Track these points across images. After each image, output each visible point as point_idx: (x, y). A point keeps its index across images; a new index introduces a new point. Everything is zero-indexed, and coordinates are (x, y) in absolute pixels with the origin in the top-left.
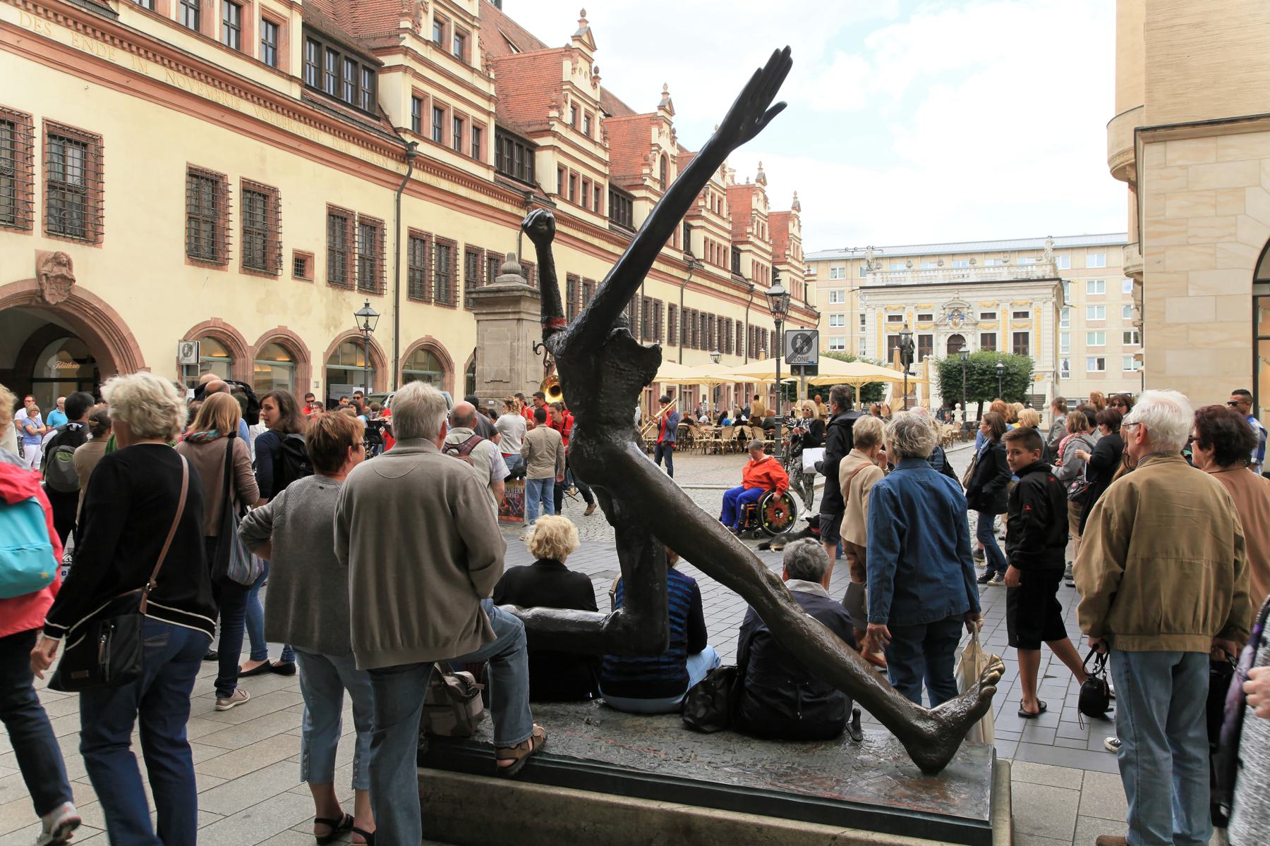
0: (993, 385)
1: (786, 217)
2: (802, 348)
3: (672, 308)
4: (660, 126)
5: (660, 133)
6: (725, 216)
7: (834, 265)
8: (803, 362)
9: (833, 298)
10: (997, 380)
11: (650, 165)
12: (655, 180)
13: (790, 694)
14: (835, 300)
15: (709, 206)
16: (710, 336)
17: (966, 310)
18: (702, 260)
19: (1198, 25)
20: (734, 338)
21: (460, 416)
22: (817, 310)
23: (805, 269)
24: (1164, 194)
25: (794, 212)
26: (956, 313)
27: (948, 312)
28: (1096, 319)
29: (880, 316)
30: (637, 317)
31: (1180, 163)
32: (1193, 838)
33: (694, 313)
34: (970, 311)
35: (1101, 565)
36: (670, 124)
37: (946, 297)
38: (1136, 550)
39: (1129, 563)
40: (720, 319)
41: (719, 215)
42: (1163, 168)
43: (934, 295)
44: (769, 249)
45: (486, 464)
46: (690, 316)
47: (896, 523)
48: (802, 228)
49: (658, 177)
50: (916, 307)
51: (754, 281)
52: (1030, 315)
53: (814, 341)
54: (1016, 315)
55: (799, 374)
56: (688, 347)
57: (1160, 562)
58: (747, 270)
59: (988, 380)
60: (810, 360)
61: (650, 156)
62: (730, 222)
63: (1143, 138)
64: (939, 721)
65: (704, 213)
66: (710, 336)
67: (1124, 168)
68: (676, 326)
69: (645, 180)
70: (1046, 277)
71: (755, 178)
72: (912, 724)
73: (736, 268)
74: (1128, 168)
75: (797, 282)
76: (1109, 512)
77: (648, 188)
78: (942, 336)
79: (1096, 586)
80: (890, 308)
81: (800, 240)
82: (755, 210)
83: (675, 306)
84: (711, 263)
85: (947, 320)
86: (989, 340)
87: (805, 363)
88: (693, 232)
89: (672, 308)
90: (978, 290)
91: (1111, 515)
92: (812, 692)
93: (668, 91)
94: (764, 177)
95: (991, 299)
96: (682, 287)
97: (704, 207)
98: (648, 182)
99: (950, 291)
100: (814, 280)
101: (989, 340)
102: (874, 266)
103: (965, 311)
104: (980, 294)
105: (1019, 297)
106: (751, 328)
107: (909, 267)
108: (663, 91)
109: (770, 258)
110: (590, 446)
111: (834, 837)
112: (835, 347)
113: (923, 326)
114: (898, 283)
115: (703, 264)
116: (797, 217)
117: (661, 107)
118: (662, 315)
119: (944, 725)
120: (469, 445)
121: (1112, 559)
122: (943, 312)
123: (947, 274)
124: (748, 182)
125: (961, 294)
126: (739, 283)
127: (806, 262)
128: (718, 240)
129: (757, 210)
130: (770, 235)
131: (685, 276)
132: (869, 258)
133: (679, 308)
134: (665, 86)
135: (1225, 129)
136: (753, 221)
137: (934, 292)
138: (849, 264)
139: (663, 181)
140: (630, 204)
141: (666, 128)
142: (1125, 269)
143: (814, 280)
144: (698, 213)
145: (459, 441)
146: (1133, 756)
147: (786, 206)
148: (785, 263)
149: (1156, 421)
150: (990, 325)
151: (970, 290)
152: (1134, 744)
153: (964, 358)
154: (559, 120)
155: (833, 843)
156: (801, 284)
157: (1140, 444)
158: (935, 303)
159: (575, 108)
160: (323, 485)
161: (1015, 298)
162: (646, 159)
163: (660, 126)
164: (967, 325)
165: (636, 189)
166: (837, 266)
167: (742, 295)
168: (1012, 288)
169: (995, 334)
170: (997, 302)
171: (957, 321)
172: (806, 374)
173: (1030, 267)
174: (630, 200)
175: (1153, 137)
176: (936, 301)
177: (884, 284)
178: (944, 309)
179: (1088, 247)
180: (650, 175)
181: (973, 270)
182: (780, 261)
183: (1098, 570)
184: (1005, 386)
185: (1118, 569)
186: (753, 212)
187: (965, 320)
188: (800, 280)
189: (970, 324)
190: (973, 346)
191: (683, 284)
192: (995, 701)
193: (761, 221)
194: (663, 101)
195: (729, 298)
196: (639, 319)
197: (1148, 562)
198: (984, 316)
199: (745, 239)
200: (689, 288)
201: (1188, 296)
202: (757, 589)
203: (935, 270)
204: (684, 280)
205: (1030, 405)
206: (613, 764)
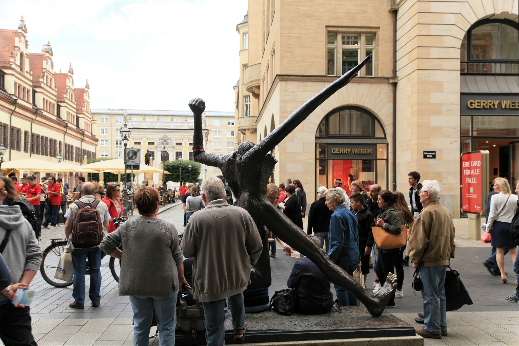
0: (187, 174)
1: (82, 91)
2: (132, 157)
3: (26, 133)
4: (20, 38)
5: (20, 41)
6: (53, 88)
8: (133, 164)
9: (102, 132)
10: (188, 172)
11: (14, 57)
12: (17, 65)
13: (320, 297)
14: (103, 133)
15: (45, 82)
16: (46, 148)
18: (42, 109)
19: (297, 38)
21: (89, 190)
22: (97, 137)
23: (91, 117)
24: (286, 101)
25: (86, 89)
26: (165, 142)
27: (162, 141)
28: (217, 147)
30: (8, 137)
31: (292, 90)
32: (444, 326)
33: (38, 136)
34: (171, 141)
35: (423, 239)
36: (25, 37)
37: (161, 135)
38: (434, 234)
39: (431, 238)
40: (51, 140)
41: (50, 87)
42: (286, 91)
44: (75, 106)
45: (103, 213)
46: (35, 138)
47: (343, 229)
48: (90, 97)
49: (19, 64)
50: (147, 139)
51: (67, 121)
52: (182, 144)
53: (138, 154)
55: (130, 169)
56: (34, 153)
57: (440, 237)
58: (64, 115)
59: (185, 172)
60: (136, 162)
61: (14, 52)
62: (56, 91)
63: (279, 79)
64: (379, 297)
65: (43, 85)
66: (46, 148)
67: (252, 87)
68: (28, 142)
69: (12, 65)
71: (68, 70)
72: (371, 300)
73: (58, 115)
74: (254, 88)
76: (424, 222)
77: (13, 69)
78: (159, 152)
79: (421, 247)
80: (135, 138)
81: (89, 103)
83: (28, 132)
84: (46, 111)
85: (161, 145)
86: (179, 154)
87: (134, 164)
88: (37, 94)
89: (26, 133)
90: (174, 132)
91: (425, 222)
92: (326, 295)
93: (23, 20)
94: (72, 71)
96: (32, 122)
97: (43, 82)
98: (13, 66)
99: (163, 132)
101: (179, 154)
102: (128, 118)
103: (169, 141)
104: (175, 134)
106: (66, 145)
107: (144, 120)
108: (21, 19)
109: (75, 111)
110: (256, 202)
111: (369, 341)
112: (103, 156)
114: (139, 127)
115: (42, 111)
116: (88, 92)
117: (20, 28)
118: (20, 137)
119: (382, 299)
120: (95, 204)
121: (426, 237)
122: (159, 141)
123: (183, 125)
124: (60, 72)
125: (167, 134)
126: (60, 122)
127: (92, 114)
128: (50, 100)
129: (69, 86)
130: (75, 99)
131: (33, 117)
132: (125, 114)
133: (30, 133)
134: (22, 17)
135: (307, 79)
136: (67, 91)
137: (155, 132)
138: (110, 116)
139: (21, 66)
140: (3, 76)
141: (23, 39)
142: (238, 128)
144: (40, 85)
145: (90, 202)
146: (430, 301)
148: (82, 114)
149: (433, 191)
151: (171, 132)
152: (431, 297)
153: (180, 163)
155: (369, 343)
157: (428, 198)
158: (156, 137)
160: (149, 221)
162: (12, 54)
163: (20, 38)
164: (170, 147)
165: (6, 69)
166: (105, 117)
167: (62, 128)
168: (189, 132)
170: (183, 138)
171: (165, 145)
172: (134, 169)
173: (190, 123)
174: (3, 74)
175: (283, 79)
177: (133, 127)
178: (160, 140)
179: (215, 117)
180: (14, 63)
181: (172, 123)
182: (79, 112)
183: (421, 241)
184: (192, 175)
185: (428, 241)
186: (67, 87)
187: (169, 145)
188: (89, 122)
190: (172, 158)
191: (32, 121)
193: (71, 92)
194: (21, 24)
195: (55, 129)
196: (9, 138)
197: (437, 237)
198: (177, 144)
199: (63, 100)
200: (35, 123)
201: (294, 142)
202: (319, 255)
203: (170, 122)
204: (33, 119)
205: (48, 183)
206: (279, 330)
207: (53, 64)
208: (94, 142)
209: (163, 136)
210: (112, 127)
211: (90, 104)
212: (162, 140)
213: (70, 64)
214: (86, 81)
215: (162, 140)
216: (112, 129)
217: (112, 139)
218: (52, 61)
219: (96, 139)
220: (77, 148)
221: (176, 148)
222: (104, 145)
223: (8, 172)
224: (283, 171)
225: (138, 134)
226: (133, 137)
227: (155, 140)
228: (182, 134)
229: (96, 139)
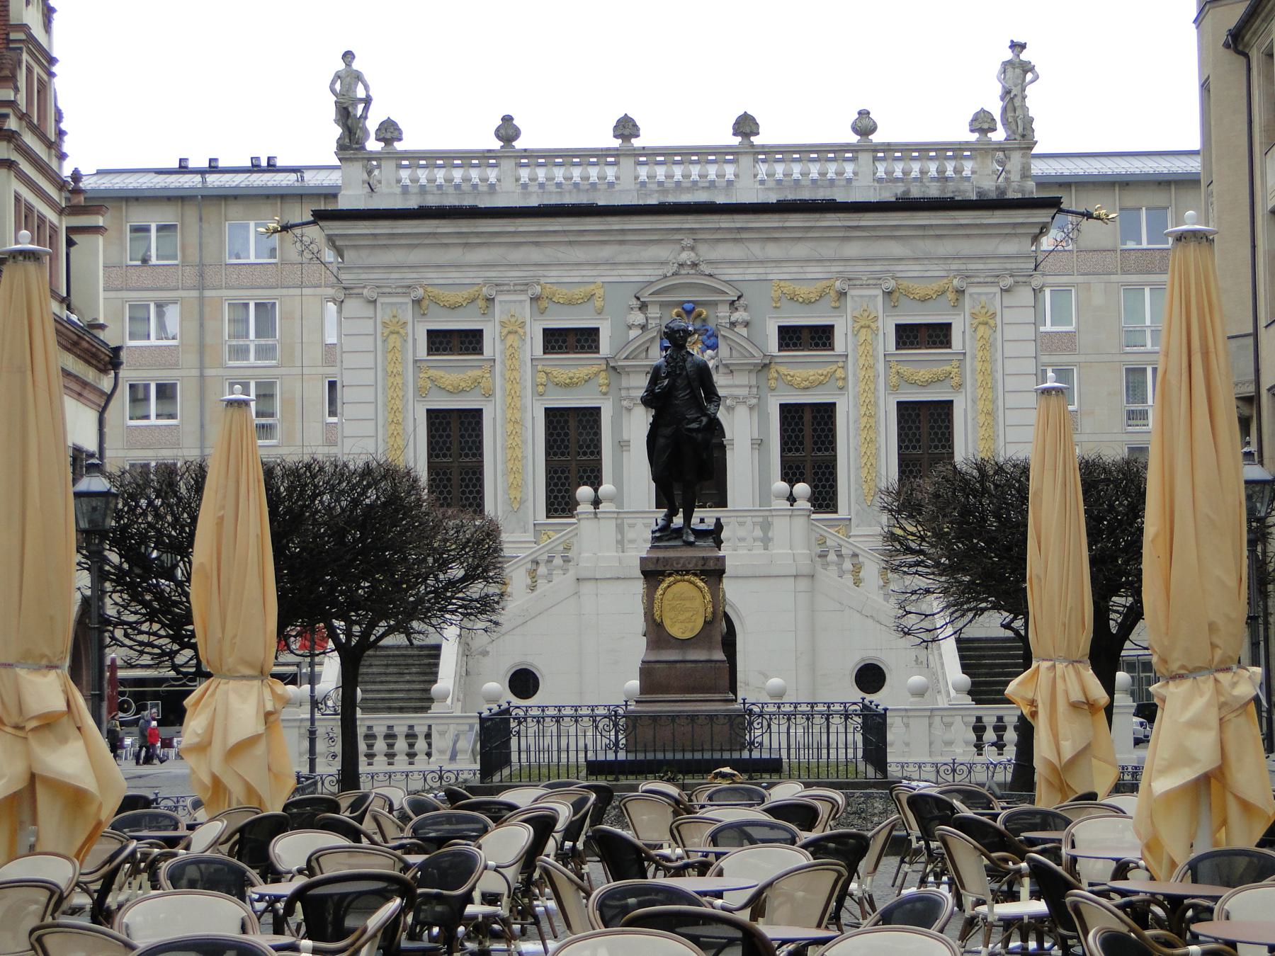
7: (139, 216)
17: (723, 312)
29: (395, 329)
34: (739, 316)
43: (606, 252)
54: (440, 341)
70: (1011, 195)
75: (42, 219)
80: (435, 301)
95: (815, 271)
100: (96, 230)
105: (914, 270)
113: (562, 374)
122: (639, 318)
137: (603, 239)
138: (191, 213)
143: (96, 230)
150: (811, 373)
151: (736, 237)
161: (554, 275)
166: (153, 218)
168: (892, 234)
169: (478, 413)
176: (612, 275)
178: (643, 307)
187: (724, 350)
188: (51, 216)
189: (742, 368)
192: (70, 469)
198: (791, 337)
208: (89, 374)
209: (669, 270)
210: (202, 287)
212: (663, 305)
215: (663, 305)
216: (201, 299)
217: (209, 372)
219: (105, 355)
221: (783, 370)
222: (153, 421)
223: (159, 595)
225: (458, 266)
226: (420, 292)
227: (600, 312)
228: (828, 250)
229: (105, 355)
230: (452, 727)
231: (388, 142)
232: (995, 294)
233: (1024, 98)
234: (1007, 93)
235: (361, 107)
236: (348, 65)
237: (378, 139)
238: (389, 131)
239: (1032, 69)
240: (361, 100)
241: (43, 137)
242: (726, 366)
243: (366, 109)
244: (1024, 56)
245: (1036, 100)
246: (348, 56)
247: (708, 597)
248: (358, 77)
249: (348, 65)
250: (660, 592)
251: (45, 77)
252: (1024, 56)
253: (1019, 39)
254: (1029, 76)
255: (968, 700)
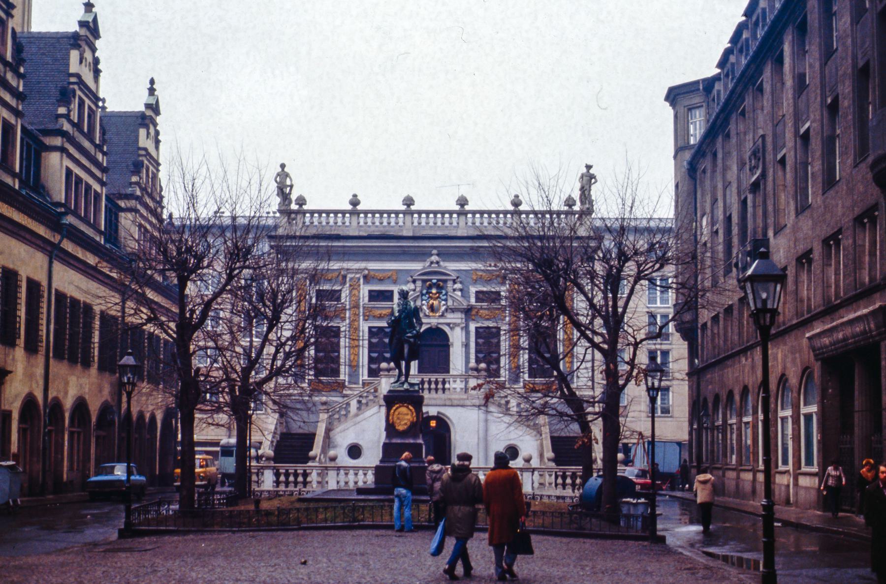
15: (75, 117)
20: (22, 312)
82: (73, 75)
147: (137, 104)
154: (67, 116)
156: (97, 196)
159: (81, 104)
178: (414, 281)
207: (160, 138)
211: (160, 168)
213: (152, 82)
214: (149, 86)
218: (97, 54)
220: (105, 317)
224: (673, 356)
230: (314, 471)
231: (301, 205)
232: (359, 279)
233: (590, 190)
234: (582, 189)
235: (288, 189)
236: (283, 170)
237: (296, 204)
238: (301, 201)
239: (595, 178)
240: (288, 186)
241: (153, 199)
242: (451, 309)
243: (291, 190)
244: (591, 171)
245: (595, 191)
246: (283, 166)
247: (414, 414)
248: (287, 175)
249: (283, 170)
250: (392, 411)
251: (155, 171)
252: (591, 171)
253: (589, 163)
254: (593, 181)
255: (552, 465)
